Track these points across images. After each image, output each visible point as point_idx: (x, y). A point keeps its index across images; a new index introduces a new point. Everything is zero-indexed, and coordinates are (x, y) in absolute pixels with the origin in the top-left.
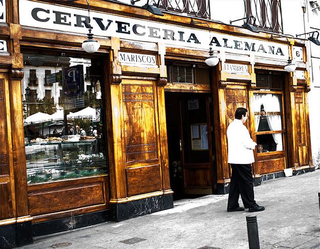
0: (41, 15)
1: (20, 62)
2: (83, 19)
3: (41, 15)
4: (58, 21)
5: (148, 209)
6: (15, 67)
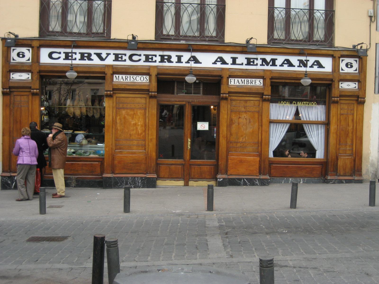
0: (54, 56)
4: (82, 58)
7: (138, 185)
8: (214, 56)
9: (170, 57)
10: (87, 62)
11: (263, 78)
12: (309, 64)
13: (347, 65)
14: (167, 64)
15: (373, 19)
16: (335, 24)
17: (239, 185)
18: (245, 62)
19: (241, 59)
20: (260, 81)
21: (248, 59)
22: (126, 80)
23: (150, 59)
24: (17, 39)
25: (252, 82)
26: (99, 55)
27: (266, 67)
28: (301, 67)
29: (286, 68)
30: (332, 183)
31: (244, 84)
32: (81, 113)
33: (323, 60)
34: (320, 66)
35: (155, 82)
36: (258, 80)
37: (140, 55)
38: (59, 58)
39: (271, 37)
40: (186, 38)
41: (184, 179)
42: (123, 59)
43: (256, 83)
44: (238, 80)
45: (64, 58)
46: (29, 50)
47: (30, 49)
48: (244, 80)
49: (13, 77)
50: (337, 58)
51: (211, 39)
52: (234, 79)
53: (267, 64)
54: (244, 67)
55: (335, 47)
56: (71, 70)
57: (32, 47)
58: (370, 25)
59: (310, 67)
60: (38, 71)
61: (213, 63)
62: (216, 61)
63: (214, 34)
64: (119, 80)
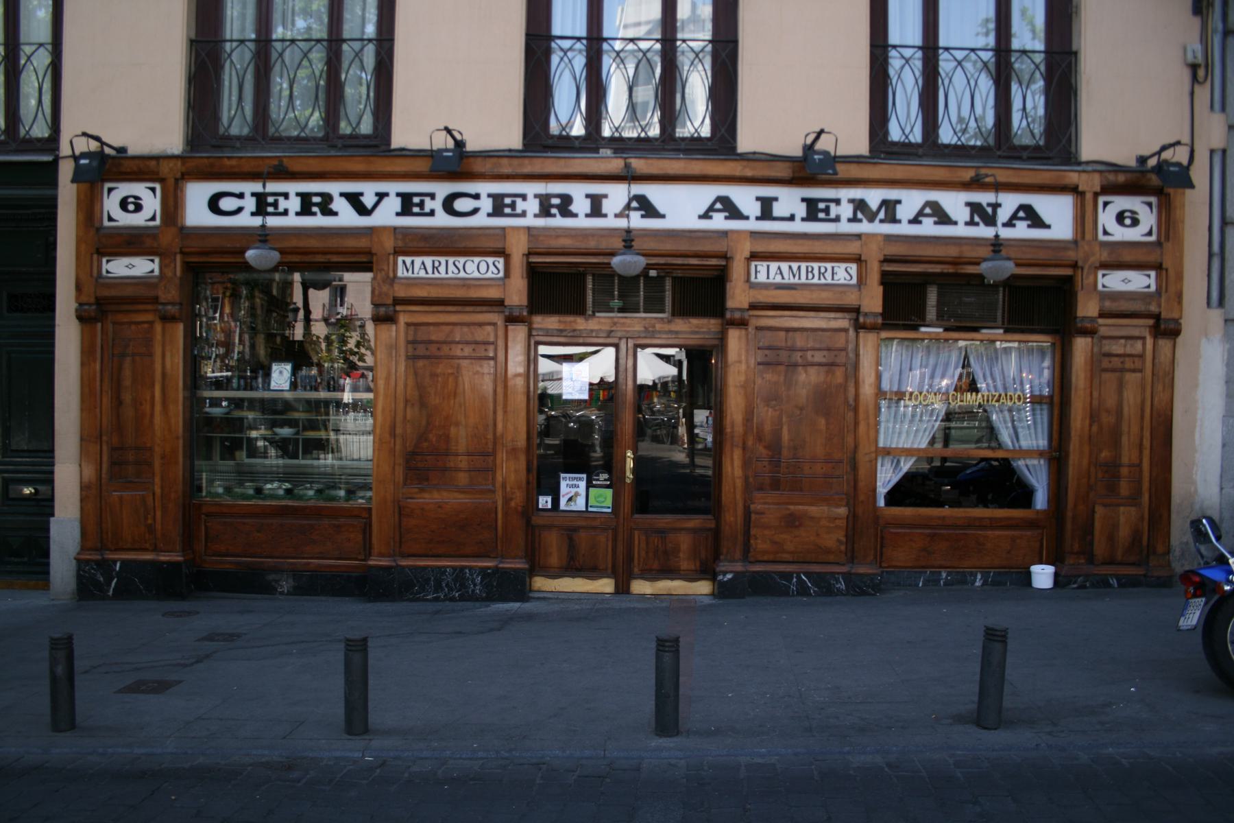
1: (174, 292)
2: (556, 201)
3: (226, 204)
4: (306, 210)
5: (451, 590)
6: (164, 301)
7: (473, 591)
8: (706, 194)
9: (567, 200)
10: (318, 221)
11: (858, 259)
12: (1003, 215)
13: (1120, 218)
14: (558, 221)
15: (1201, 73)
16: (1079, 93)
17: (785, 592)
18: (801, 210)
19: (789, 201)
20: (849, 269)
21: (811, 204)
22: (433, 273)
23: (822, 211)
24: (122, 158)
25: (823, 274)
26: (354, 200)
27: (864, 227)
28: (977, 224)
29: (929, 227)
30: (1075, 586)
31: (799, 278)
32: (938, 354)
33: (1047, 205)
34: (1035, 220)
35: (522, 277)
36: (843, 265)
37: (477, 197)
38: (239, 210)
39: (881, 135)
40: (619, 145)
41: (614, 574)
42: (427, 210)
43: (836, 277)
44: (779, 268)
45: (490, 211)
46: (153, 190)
47: (158, 186)
48: (799, 268)
49: (110, 270)
50: (1089, 196)
51: (695, 146)
52: (768, 263)
53: (872, 217)
54: (798, 227)
55: (1080, 164)
56: (261, 241)
57: (162, 181)
58: (1192, 94)
59: (1004, 225)
60: (527, 252)
61: (701, 217)
62: (711, 209)
63: (706, 132)
64: (413, 273)
